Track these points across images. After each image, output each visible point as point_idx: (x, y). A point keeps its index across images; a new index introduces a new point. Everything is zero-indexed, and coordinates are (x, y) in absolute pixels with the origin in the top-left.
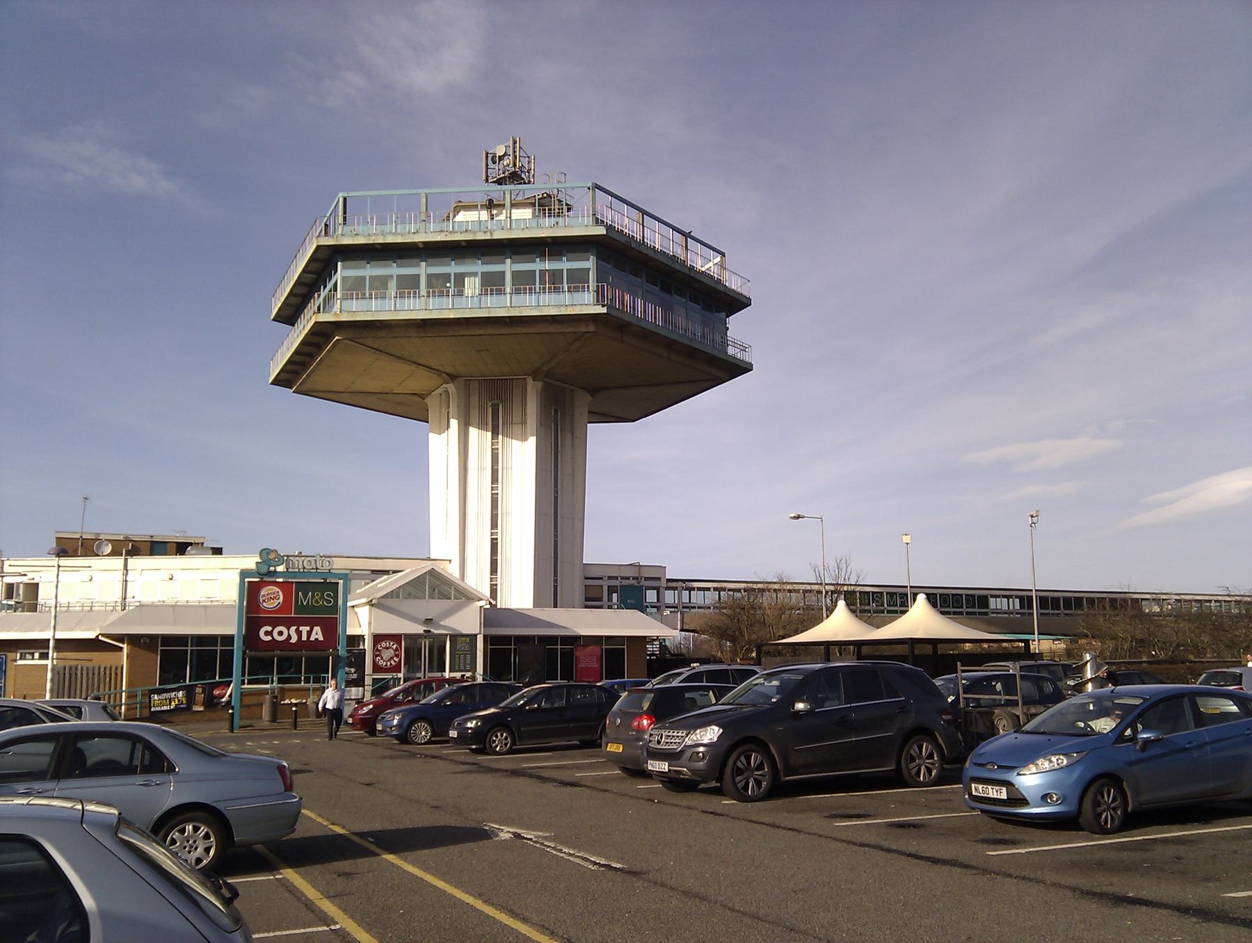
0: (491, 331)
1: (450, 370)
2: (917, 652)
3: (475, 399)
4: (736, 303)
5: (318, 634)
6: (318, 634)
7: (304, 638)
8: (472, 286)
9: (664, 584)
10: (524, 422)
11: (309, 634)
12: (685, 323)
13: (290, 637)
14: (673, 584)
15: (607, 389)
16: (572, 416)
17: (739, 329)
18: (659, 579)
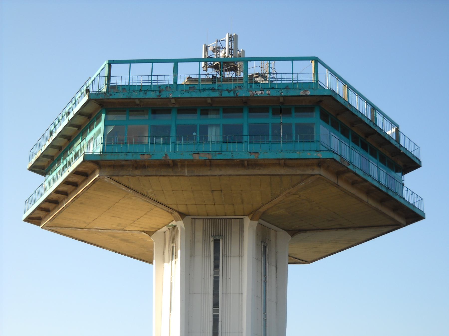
0: (230, 172)
1: (182, 209)
4: (410, 164)
10: (241, 255)
12: (376, 173)
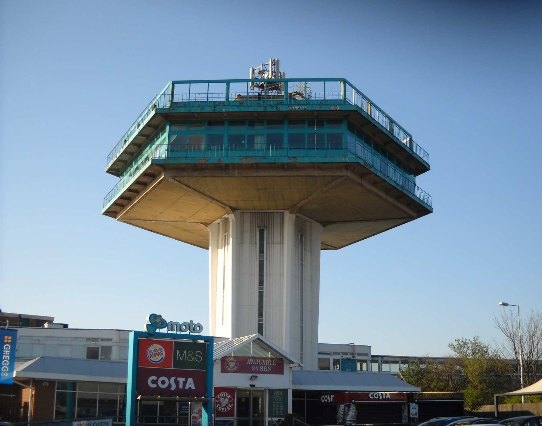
0: (273, 173)
1: (233, 204)
2: (500, 410)
3: (247, 226)
5: (191, 384)
6: (191, 384)
7: (181, 387)
8: (260, 142)
9: (370, 358)
10: (282, 243)
11: (185, 383)
13: (170, 385)
14: (375, 359)
15: (335, 222)
16: (311, 240)
17: (424, 186)
18: (366, 355)
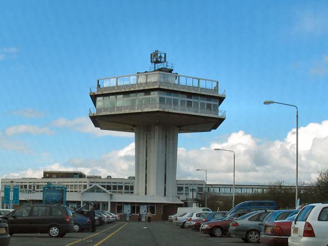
10: (154, 138)
